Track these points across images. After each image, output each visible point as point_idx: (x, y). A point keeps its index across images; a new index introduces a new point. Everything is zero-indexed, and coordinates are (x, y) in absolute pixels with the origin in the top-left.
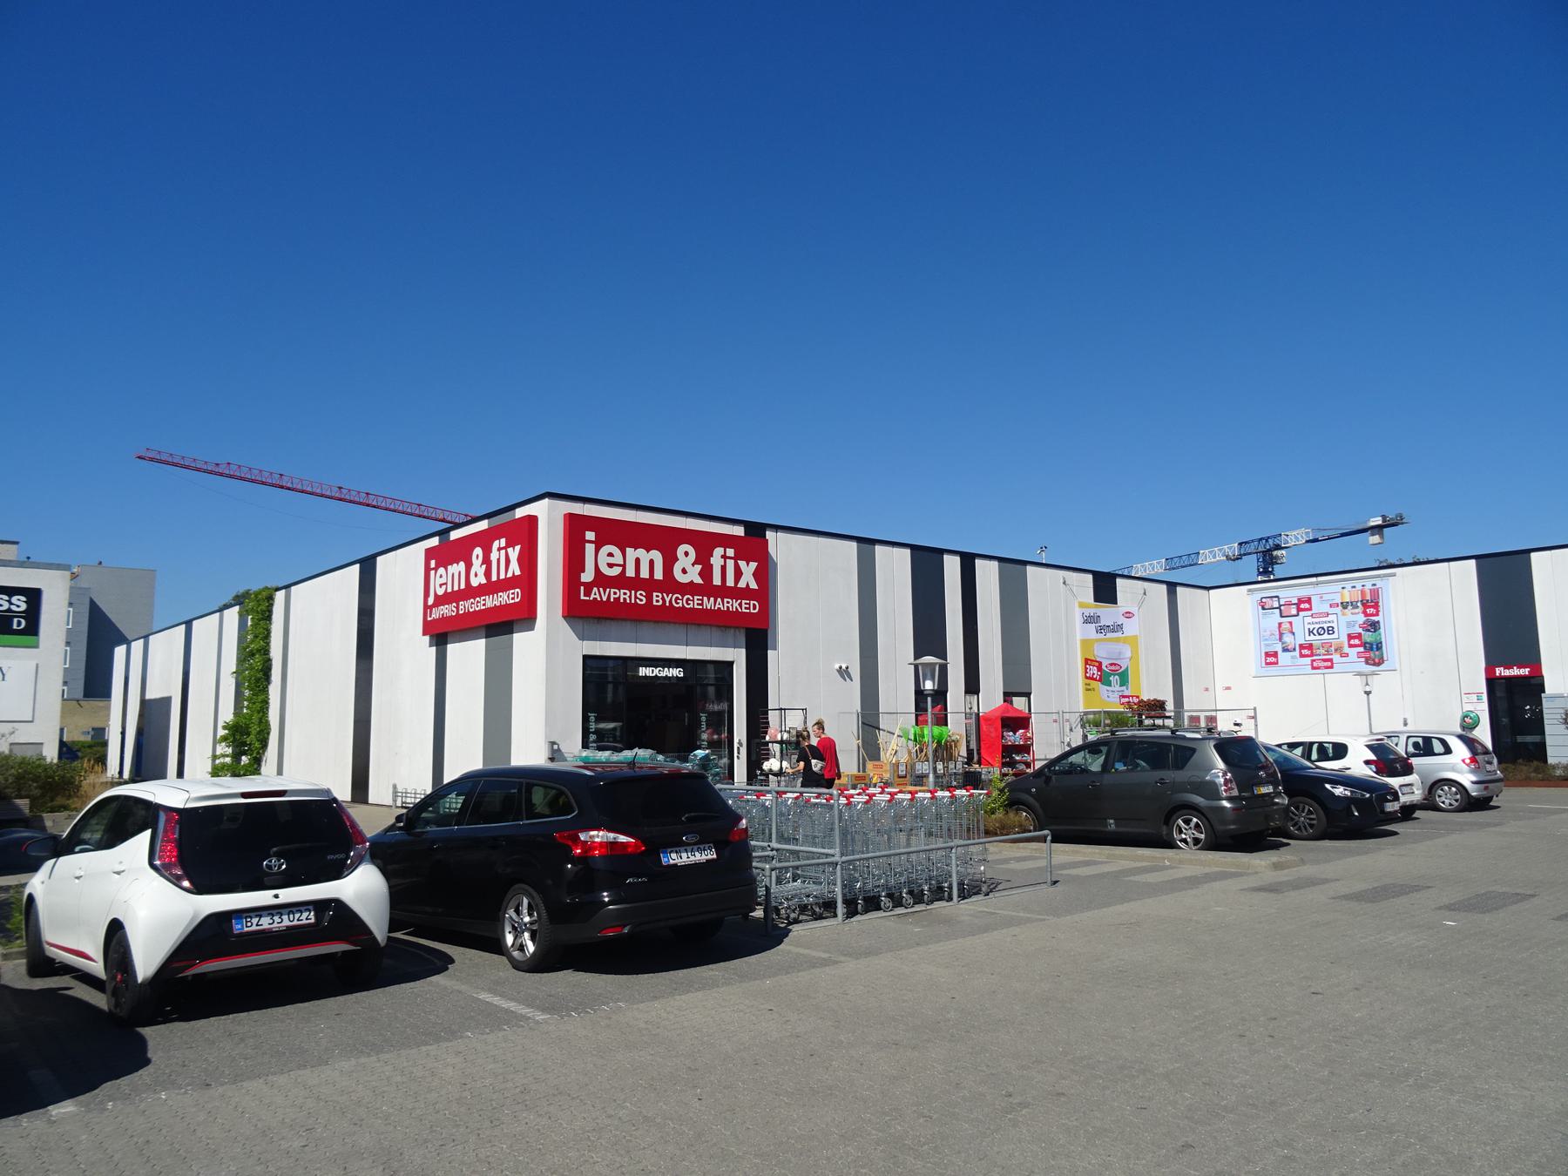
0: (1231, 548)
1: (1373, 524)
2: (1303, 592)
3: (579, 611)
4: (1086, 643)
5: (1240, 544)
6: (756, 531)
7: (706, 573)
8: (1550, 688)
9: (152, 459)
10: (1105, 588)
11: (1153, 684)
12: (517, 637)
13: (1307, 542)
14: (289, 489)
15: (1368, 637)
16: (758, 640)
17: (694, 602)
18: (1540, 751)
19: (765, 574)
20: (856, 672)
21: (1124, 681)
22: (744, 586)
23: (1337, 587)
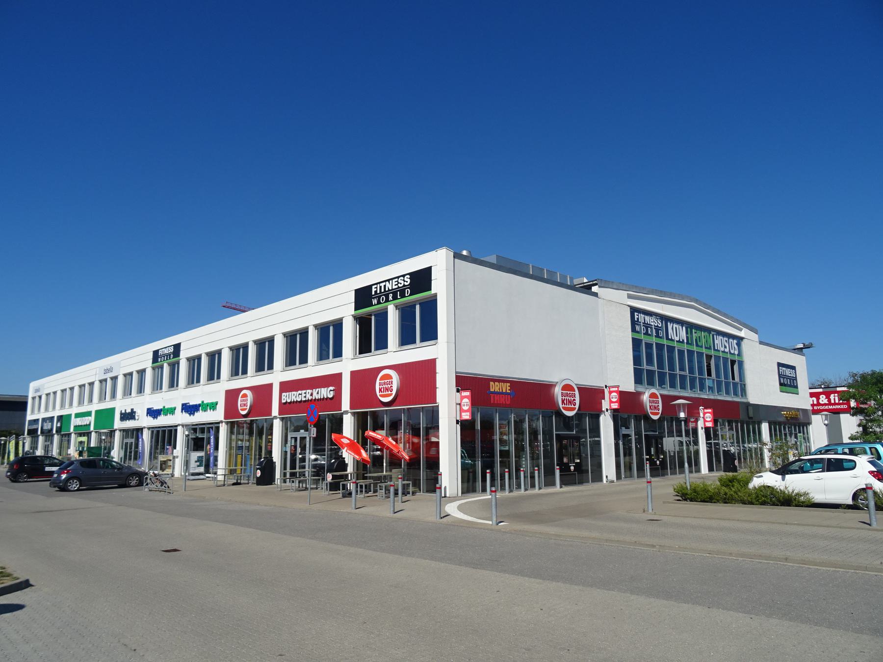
1: (798, 347)
7: (829, 400)
12: (841, 415)
17: (827, 407)
18: (630, 309)
22: (130, 411)
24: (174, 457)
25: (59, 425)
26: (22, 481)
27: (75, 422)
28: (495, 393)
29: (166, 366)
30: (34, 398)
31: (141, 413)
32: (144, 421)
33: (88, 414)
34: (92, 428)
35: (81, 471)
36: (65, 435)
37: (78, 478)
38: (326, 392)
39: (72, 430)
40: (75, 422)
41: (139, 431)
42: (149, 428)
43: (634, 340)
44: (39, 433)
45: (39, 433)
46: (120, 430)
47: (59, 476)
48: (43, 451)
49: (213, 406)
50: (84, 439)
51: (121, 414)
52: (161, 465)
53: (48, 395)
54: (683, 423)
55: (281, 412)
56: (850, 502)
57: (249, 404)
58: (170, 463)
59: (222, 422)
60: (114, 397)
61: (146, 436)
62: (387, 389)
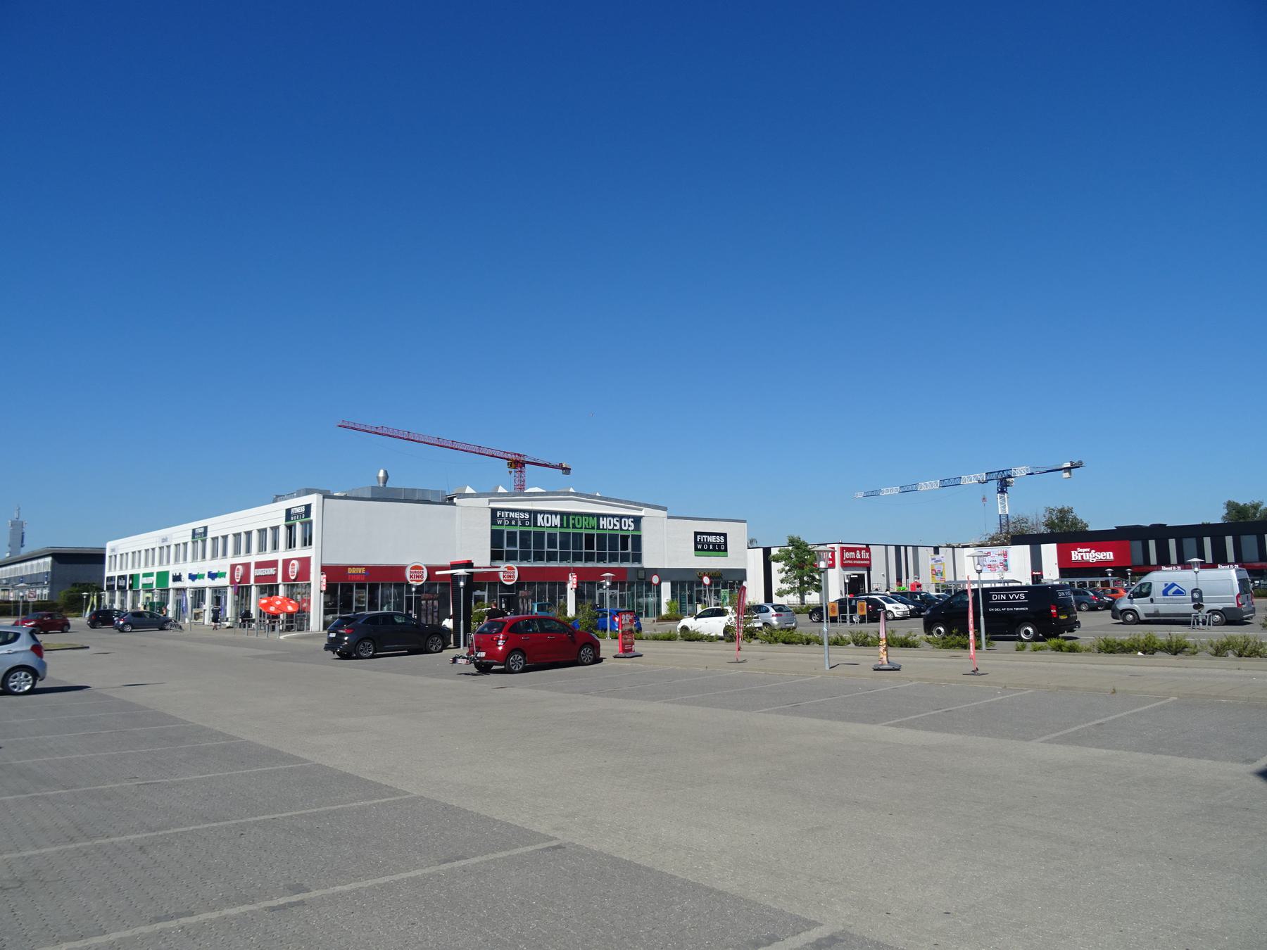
0: (981, 476)
2: (988, 551)
3: (845, 566)
5: (987, 474)
6: (867, 545)
8: (1044, 577)
10: (936, 550)
11: (949, 577)
13: (1027, 474)
15: (1005, 563)
16: (869, 569)
19: (870, 555)
21: (942, 575)
23: (997, 550)
24: (205, 610)
25: (131, 583)
27: (143, 581)
28: (351, 574)
29: (199, 541)
30: (110, 557)
31: (185, 576)
32: (186, 583)
33: (151, 575)
34: (154, 587)
35: (132, 619)
36: (136, 591)
38: (271, 571)
39: (140, 587)
40: (143, 581)
41: (184, 590)
42: (210, 588)
43: (493, 532)
44: (116, 589)
45: (116, 589)
46: (173, 589)
47: (119, 622)
48: (120, 605)
49: (223, 575)
50: (149, 595)
51: (173, 576)
52: (195, 616)
53: (122, 555)
54: (462, 590)
55: (256, 582)
56: (721, 634)
57: (296, 572)
58: (202, 615)
59: (228, 586)
60: (275, 549)
61: (189, 595)
62: (510, 577)
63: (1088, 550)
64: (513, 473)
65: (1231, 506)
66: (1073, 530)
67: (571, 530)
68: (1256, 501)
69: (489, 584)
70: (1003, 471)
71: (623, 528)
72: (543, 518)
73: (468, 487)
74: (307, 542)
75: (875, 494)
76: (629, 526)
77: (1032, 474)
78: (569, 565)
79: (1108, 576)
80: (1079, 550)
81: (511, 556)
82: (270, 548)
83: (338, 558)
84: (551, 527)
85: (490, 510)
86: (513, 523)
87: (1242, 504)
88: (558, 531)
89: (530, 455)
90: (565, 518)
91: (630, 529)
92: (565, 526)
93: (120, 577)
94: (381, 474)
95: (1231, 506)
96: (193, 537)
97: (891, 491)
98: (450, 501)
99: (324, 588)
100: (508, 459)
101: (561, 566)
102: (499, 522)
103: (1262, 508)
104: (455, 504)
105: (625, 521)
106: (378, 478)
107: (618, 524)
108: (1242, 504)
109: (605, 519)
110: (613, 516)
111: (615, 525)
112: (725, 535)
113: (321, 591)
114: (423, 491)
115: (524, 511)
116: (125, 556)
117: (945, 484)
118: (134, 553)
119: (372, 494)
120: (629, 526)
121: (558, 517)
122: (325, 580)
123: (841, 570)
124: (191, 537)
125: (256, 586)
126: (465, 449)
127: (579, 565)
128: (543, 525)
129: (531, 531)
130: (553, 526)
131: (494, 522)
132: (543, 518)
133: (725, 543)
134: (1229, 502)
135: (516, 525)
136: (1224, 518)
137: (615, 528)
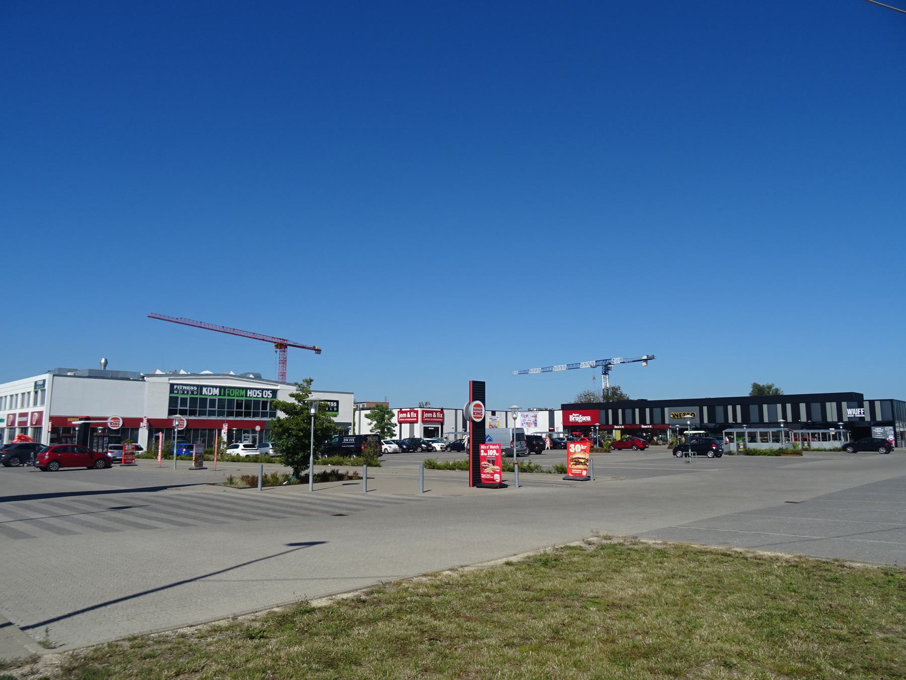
3: (423, 422)
4: (490, 422)
5: (596, 361)
6: (442, 409)
7: (437, 416)
9: (153, 317)
12: (415, 424)
14: (204, 328)
16: (442, 424)
19: (443, 416)
20: (454, 428)
26: (14, 465)
34: (29, 425)
37: (59, 462)
43: (171, 398)
62: (479, 414)
63: (578, 415)
64: (278, 352)
65: (755, 386)
66: (621, 399)
67: (226, 398)
68: (770, 384)
69: (167, 429)
70: (606, 360)
71: (264, 396)
72: (207, 390)
73: (182, 370)
74: (43, 403)
75: (525, 372)
76: (268, 395)
77: (624, 362)
78: (223, 419)
79: (840, 429)
80: (574, 414)
81: (183, 413)
82: (40, 403)
83: (61, 412)
84: (212, 395)
85: (169, 385)
86: (186, 392)
87: (762, 385)
88: (217, 398)
89: (292, 340)
90: (222, 390)
91: (269, 397)
92: (222, 394)
93: (22, 415)
94: (103, 361)
95: (755, 386)
96: (35, 388)
97: (560, 368)
98: (142, 379)
99: (50, 430)
100: (275, 343)
101: (208, 419)
102: (176, 392)
103: (773, 388)
104: (144, 381)
105: (265, 393)
106: (101, 363)
107: (261, 394)
108: (762, 385)
109: (251, 391)
110: (257, 389)
111: (258, 395)
112: (337, 402)
113: (49, 432)
114: (125, 372)
115: (193, 385)
116: (14, 397)
117: (544, 371)
118: (12, 396)
119: (89, 373)
120: (268, 395)
121: (218, 389)
122: (50, 425)
123: (422, 424)
124: (33, 388)
125: (31, 427)
126: (243, 335)
127: (231, 418)
128: (206, 394)
129: (198, 398)
130: (214, 394)
131: (172, 391)
132: (207, 390)
133: (337, 407)
134: (754, 383)
135: (188, 393)
136: (750, 394)
137: (258, 396)
